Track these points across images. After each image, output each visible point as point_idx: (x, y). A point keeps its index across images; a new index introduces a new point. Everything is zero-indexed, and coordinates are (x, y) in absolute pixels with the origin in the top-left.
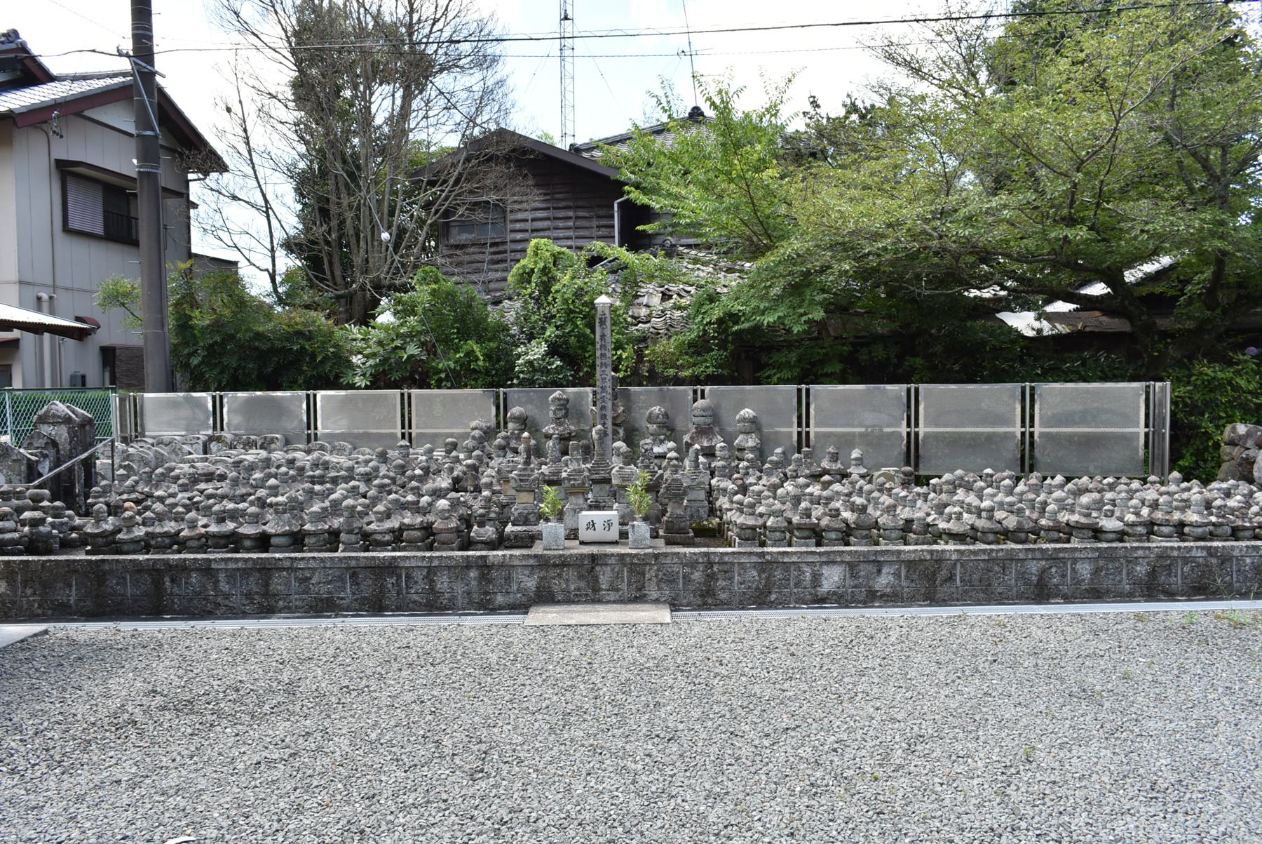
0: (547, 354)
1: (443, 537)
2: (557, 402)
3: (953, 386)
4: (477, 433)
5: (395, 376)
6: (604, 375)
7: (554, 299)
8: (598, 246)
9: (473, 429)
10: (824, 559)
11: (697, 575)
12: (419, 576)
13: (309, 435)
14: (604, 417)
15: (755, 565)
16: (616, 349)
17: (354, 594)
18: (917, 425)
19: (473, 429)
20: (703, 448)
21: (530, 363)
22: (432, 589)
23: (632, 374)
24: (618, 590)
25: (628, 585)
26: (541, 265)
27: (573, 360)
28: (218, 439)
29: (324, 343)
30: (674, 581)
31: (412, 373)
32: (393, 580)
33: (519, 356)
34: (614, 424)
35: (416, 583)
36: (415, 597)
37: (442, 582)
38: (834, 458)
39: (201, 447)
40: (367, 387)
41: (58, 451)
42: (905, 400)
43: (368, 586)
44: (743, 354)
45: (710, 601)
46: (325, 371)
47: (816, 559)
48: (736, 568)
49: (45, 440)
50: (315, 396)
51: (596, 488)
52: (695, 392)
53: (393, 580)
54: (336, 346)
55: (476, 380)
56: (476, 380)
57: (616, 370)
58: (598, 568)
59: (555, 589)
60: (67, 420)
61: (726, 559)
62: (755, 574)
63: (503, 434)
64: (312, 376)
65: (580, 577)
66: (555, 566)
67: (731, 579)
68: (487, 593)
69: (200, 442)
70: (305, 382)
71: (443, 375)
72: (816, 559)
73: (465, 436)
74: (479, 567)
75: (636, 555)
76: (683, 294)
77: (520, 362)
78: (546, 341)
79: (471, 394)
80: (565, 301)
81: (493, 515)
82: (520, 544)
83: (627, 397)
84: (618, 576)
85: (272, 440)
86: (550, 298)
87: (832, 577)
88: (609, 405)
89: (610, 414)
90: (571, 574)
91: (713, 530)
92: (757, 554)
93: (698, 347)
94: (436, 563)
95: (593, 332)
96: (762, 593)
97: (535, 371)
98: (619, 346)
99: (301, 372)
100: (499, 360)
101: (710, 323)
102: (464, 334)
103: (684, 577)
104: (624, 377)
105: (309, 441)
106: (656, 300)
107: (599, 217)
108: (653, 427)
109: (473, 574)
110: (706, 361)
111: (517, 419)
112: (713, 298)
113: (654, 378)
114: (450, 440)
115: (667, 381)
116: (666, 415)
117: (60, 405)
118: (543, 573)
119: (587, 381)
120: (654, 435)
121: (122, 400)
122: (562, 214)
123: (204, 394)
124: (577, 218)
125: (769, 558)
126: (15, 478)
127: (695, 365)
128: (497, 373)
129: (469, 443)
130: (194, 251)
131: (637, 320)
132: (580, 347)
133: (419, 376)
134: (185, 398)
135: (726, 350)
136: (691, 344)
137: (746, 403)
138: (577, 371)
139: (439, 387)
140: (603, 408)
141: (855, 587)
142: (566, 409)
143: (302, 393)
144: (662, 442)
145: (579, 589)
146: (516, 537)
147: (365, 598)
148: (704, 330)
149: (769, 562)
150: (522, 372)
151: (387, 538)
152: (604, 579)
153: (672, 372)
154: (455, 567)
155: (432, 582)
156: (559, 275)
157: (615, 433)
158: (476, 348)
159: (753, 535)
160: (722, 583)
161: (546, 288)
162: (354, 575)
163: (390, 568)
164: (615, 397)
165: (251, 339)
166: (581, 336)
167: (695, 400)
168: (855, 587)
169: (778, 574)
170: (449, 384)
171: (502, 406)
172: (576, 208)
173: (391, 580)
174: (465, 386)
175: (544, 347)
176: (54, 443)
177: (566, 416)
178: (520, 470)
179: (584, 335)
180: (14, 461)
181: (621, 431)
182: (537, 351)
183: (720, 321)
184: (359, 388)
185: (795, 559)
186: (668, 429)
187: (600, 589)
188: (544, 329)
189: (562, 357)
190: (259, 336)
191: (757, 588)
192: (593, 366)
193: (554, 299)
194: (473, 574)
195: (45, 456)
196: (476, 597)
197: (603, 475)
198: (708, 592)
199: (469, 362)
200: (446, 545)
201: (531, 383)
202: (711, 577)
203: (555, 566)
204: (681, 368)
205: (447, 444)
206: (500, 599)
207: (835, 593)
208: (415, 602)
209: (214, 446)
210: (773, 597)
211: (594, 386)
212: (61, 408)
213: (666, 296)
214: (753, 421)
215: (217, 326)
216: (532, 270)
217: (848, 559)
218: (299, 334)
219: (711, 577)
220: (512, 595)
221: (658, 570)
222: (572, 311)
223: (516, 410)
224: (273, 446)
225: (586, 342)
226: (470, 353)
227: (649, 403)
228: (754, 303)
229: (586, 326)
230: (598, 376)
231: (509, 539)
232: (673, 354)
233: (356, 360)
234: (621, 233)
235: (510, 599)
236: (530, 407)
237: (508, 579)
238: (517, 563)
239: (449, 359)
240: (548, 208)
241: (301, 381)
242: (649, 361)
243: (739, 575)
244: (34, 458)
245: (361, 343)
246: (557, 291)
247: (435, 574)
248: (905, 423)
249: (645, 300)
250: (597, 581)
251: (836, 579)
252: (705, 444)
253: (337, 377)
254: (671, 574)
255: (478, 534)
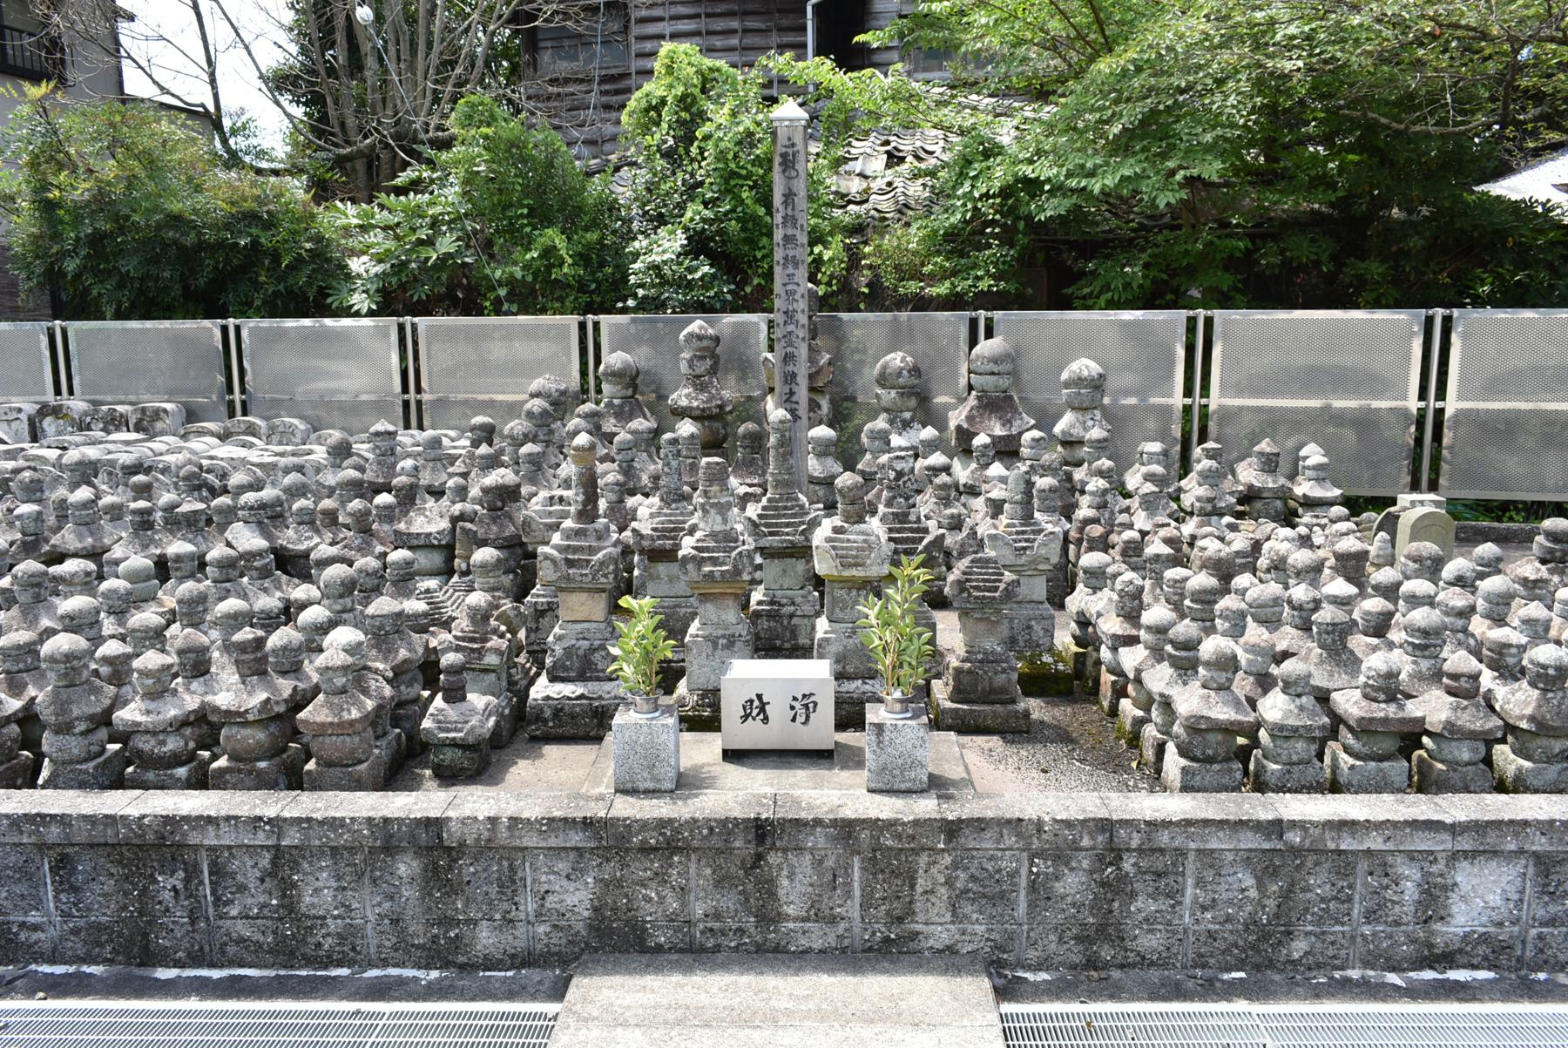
0: (685, 253)
1: (332, 745)
2: (696, 343)
3: (1528, 314)
4: (537, 405)
5: (422, 292)
6: (793, 287)
7: (702, 150)
8: (779, 62)
9: (533, 396)
10: (1465, 843)
11: (1072, 884)
12: (248, 871)
13: (231, 404)
14: (790, 378)
15: (1249, 859)
16: (812, 244)
17: (66, 915)
18: (1441, 394)
19: (533, 396)
20: (996, 440)
21: (656, 267)
22: (290, 907)
23: (840, 291)
24: (833, 920)
25: (865, 906)
26: (680, 90)
27: (734, 264)
28: (56, 412)
29: (294, 233)
30: (1002, 895)
31: (451, 288)
32: (177, 880)
33: (636, 255)
34: (812, 389)
35: (242, 888)
36: (243, 929)
37: (319, 891)
38: (1270, 464)
40: (371, 313)
43: (104, 900)
44: (1048, 256)
45: (1106, 953)
46: (309, 288)
47: (1441, 844)
48: (1191, 864)
50: (238, 329)
51: (773, 569)
52: (973, 323)
53: (177, 880)
54: (319, 239)
55: (561, 299)
56: (561, 299)
57: (812, 279)
58: (774, 858)
59: (649, 912)
61: (1164, 838)
62: (1250, 881)
63: (589, 407)
64: (276, 294)
65: (722, 881)
66: (646, 850)
67: (1174, 894)
68: (447, 922)
69: (24, 416)
70: (264, 302)
71: (502, 292)
72: (1441, 844)
73: (512, 409)
74: (421, 851)
75: (891, 824)
76: (923, 155)
77: (636, 266)
78: (686, 229)
80: (721, 156)
81: (491, 660)
82: (568, 730)
83: (836, 332)
84: (834, 880)
85: (157, 414)
86: (694, 150)
87: (1482, 896)
88: (803, 351)
89: (802, 370)
90: (698, 874)
91: (1057, 677)
92: (1258, 826)
93: (960, 242)
94: (292, 838)
95: (770, 212)
96: (1265, 936)
97: (665, 282)
98: (816, 238)
99: (257, 286)
100: (602, 264)
101: (986, 196)
102: (542, 217)
103: (1033, 887)
104: (826, 296)
105: (232, 415)
106: (878, 164)
107: (781, 30)
108: (889, 396)
109: (407, 867)
110: (975, 266)
111: (616, 375)
112: (991, 151)
113: (878, 298)
114: (479, 419)
115: (901, 303)
116: (915, 371)
118: (610, 870)
119: (758, 301)
120: (892, 412)
122: (720, 25)
123: (207, 323)
124: (746, 31)
125: (1294, 837)
127: (954, 273)
128: (598, 286)
129: (517, 426)
130: (127, 91)
131: (845, 199)
132: (745, 240)
133: (460, 293)
135: (1012, 246)
136: (951, 235)
137: (1089, 343)
138: (741, 285)
139: (498, 313)
140: (788, 358)
141: (1552, 922)
142: (714, 356)
143: (573, 320)
144: (906, 425)
145: (717, 916)
146: (557, 712)
147: (98, 927)
148: (975, 209)
149: (1295, 851)
150: (642, 286)
151: (173, 744)
152: (794, 887)
153: (913, 286)
154: (351, 850)
155: (287, 889)
156: (710, 107)
157: (814, 406)
158: (560, 242)
159: (1227, 755)
160: (1144, 905)
161: (686, 132)
162: (63, 864)
163: (163, 845)
164: (813, 333)
165: (159, 227)
166: (748, 221)
167: (973, 342)
168: (1552, 922)
169: (1319, 884)
170: (514, 308)
171: (589, 349)
172: (745, 14)
173: (167, 883)
174: (543, 311)
175: (680, 240)
177: (713, 371)
178: (569, 534)
179: (755, 218)
181: (825, 404)
182: (668, 244)
183: (1005, 192)
184: (357, 314)
185: (1375, 842)
186: (917, 401)
187: (780, 917)
188: (681, 207)
189: (714, 260)
190: (176, 220)
191: (1252, 923)
192: (769, 276)
193: (702, 150)
194: (407, 867)
196: (419, 932)
197: (791, 536)
198: (1101, 929)
199: (549, 268)
200: (342, 774)
201: (652, 305)
202: (1115, 889)
203: (646, 850)
204: (932, 279)
205: (473, 429)
206: (486, 939)
207: (1485, 938)
208: (241, 941)
209: (49, 424)
210: (1299, 947)
211: (771, 311)
213: (894, 159)
214: (1097, 385)
215: (101, 201)
216: (663, 102)
217: (1539, 844)
218: (252, 217)
219: (1115, 889)
220: (521, 930)
221: (955, 866)
222: (734, 175)
223: (614, 359)
224: (159, 425)
225: (757, 230)
226: (549, 252)
227: (881, 348)
228: (1075, 160)
229: (758, 201)
230: (778, 287)
231: (538, 717)
232: (915, 253)
233: (356, 265)
234: (819, 33)
235: (518, 939)
236: (644, 351)
237: (510, 884)
238: (531, 840)
239: (515, 263)
240: (698, 16)
241: (257, 303)
242: (870, 267)
243: (1200, 883)
245: (362, 235)
246: (707, 138)
247: (295, 866)
249: (857, 166)
250: (772, 894)
251: (1495, 899)
252: (999, 431)
253: (323, 293)
254: (995, 876)
255: (442, 725)
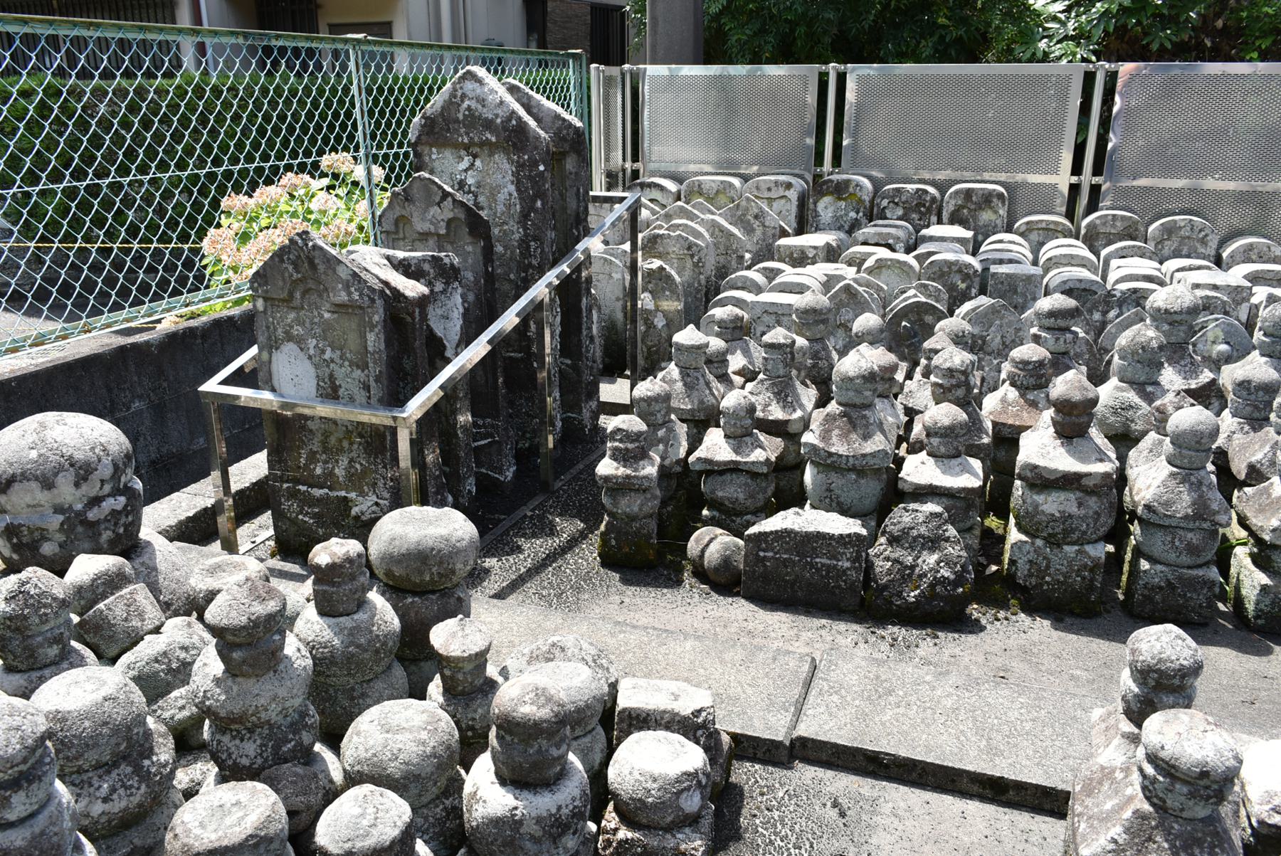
39: (793, 208)
41: (488, 253)
42: (811, 117)
49: (447, 211)
50: (842, 78)
52: (467, 58)
60: (513, 136)
69: (793, 195)
79: (909, 78)
117: (491, 81)
121: (609, 82)
126: (349, 379)
134: (1122, 95)
176: (474, 224)
180: (339, 308)
195: (449, 274)
212: (495, 90)
244: (412, 288)
248: (1067, 158)
